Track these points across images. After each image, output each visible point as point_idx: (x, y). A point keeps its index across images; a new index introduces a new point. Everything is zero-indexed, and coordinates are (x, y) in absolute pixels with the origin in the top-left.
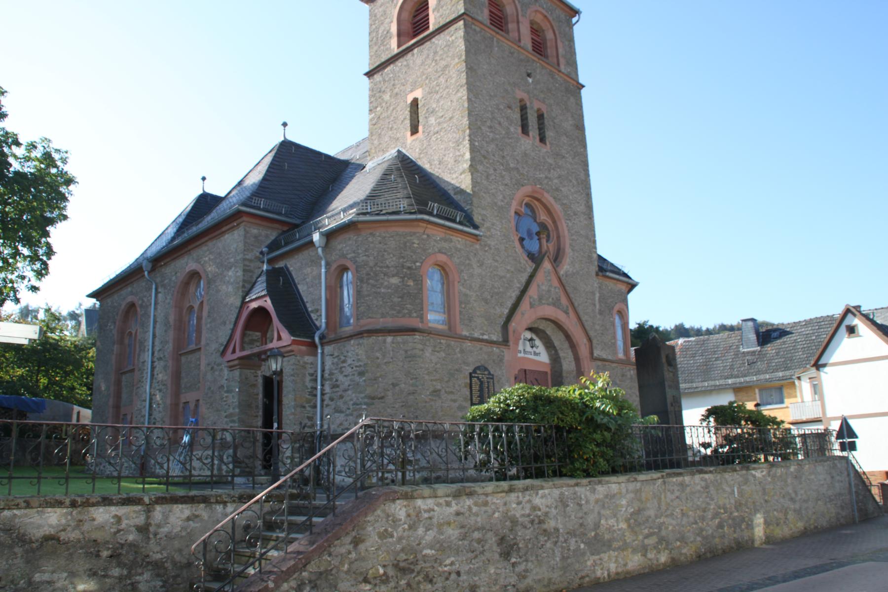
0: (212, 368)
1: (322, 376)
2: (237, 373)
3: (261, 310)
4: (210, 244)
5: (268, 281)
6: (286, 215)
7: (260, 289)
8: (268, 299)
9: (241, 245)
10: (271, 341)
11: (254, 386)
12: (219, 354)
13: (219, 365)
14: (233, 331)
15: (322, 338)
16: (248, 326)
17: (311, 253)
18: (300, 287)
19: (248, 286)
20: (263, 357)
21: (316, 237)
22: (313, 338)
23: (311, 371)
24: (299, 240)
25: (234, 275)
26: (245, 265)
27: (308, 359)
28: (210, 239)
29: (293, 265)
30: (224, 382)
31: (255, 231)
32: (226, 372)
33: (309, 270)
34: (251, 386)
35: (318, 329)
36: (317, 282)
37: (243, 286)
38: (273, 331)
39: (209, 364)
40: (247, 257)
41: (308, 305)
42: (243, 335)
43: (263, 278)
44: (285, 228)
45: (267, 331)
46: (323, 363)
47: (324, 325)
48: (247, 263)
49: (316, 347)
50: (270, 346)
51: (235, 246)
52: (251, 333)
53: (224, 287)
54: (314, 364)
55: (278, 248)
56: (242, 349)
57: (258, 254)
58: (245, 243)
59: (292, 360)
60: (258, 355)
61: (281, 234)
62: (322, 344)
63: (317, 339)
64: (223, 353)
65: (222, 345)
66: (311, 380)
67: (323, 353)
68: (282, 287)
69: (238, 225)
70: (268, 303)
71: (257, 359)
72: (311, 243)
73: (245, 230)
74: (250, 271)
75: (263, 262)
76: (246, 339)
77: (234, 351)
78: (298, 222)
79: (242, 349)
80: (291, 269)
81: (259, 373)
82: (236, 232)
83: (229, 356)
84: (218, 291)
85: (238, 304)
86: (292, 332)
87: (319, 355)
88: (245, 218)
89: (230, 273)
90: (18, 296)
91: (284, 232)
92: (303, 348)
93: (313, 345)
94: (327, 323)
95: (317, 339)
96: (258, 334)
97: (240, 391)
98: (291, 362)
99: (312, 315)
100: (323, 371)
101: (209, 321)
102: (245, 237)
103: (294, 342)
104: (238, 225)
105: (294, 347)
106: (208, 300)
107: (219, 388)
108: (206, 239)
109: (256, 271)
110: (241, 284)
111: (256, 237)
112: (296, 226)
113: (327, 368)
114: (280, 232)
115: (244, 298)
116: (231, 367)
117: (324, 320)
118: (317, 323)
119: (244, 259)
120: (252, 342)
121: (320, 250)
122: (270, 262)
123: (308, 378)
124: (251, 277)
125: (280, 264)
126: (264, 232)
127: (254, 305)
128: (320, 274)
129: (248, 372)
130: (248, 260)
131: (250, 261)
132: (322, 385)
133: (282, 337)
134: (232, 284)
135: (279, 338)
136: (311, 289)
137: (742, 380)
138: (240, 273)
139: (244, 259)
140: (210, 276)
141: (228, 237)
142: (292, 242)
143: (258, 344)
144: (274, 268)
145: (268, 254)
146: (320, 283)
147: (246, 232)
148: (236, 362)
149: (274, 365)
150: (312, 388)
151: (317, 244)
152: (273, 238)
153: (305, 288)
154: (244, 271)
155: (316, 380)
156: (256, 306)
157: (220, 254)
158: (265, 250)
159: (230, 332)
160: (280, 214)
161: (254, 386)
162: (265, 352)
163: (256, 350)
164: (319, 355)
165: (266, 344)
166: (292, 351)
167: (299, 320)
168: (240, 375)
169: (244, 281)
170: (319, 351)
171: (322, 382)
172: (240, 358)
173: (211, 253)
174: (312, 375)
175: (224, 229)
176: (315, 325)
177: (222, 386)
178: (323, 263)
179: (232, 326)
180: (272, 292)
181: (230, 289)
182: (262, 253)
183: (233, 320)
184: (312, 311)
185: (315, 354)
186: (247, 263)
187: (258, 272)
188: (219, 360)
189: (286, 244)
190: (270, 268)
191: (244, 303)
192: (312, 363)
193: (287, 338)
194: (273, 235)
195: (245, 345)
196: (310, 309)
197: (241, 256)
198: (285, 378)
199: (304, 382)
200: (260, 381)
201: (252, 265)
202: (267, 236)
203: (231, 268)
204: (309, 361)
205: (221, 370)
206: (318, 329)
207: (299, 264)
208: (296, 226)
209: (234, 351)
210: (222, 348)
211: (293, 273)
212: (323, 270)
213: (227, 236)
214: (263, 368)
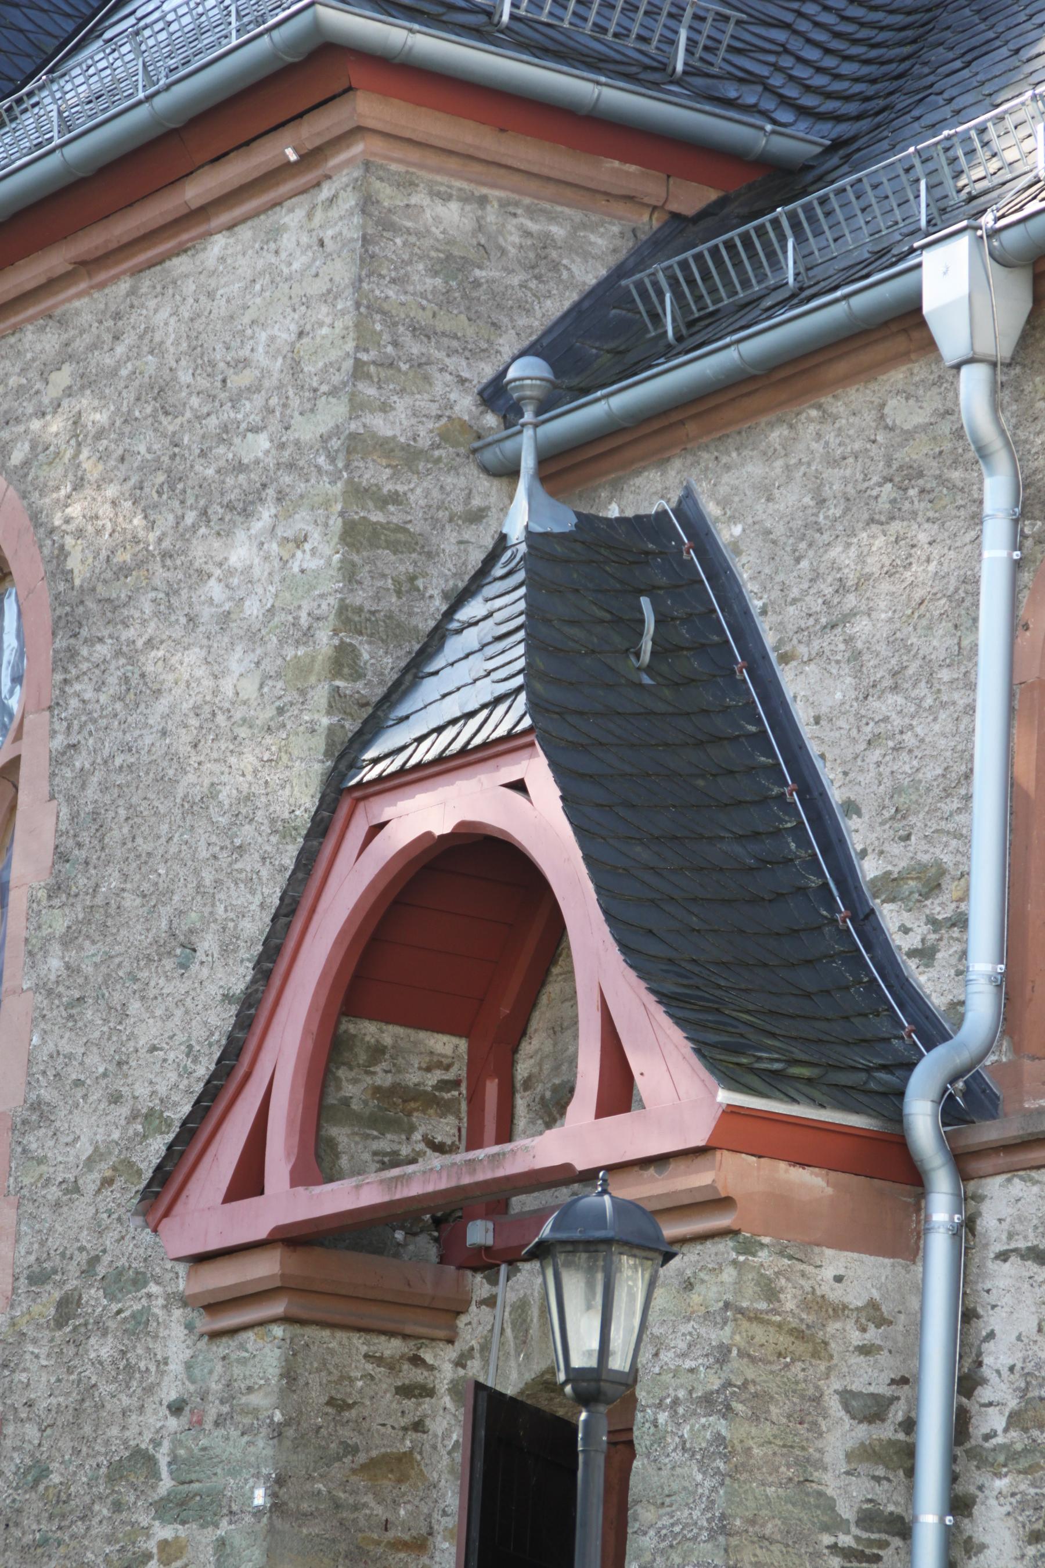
0: (67, 1308)
1: (959, 1426)
2: (264, 1354)
3: (482, 859)
4: (85, 307)
5: (539, 630)
6: (701, 85)
7: (479, 678)
8: (536, 768)
9: (333, 336)
10: (554, 1109)
11: (399, 1466)
12: (126, 1195)
13: (126, 1281)
14: (252, 1012)
15: (966, 1104)
16: (367, 981)
17: (904, 414)
18: (795, 684)
19: (383, 662)
20: (479, 1233)
21: (949, 280)
22: (891, 1102)
23: (870, 1378)
24: (799, 296)
25: (275, 565)
26: (357, 492)
27: (850, 1274)
28: (88, 266)
29: (760, 505)
30: (154, 1425)
31: (445, 215)
32: (175, 1341)
33: (877, 545)
34: (371, 1467)
35: (933, 1031)
36: (939, 643)
37: (344, 661)
38: (566, 1027)
39: (39, 1278)
40: (381, 425)
41: (857, 834)
42: (329, 1052)
43: (503, 604)
44: (692, 197)
45: (516, 1032)
46: (966, 1316)
47: (981, 1009)
48: (375, 473)
49: (915, 1179)
50: (542, 1149)
51: (284, 332)
52: (389, 1034)
53: (190, 661)
54: (889, 1322)
55: (629, 367)
56: (317, 1163)
57: (465, 404)
58: (367, 308)
59: (712, 1274)
60: (441, 1218)
61: (654, 247)
62: (964, 1163)
63: (921, 1117)
64: (162, 1191)
65: (152, 1118)
66: (865, 1454)
67: (967, 1229)
68: (659, 679)
69: (311, 157)
70: (537, 815)
71: (426, 1247)
72: (905, 324)
73: (367, 204)
74: (401, 540)
75: (510, 472)
76: (353, 1088)
77: (248, 1182)
78: (794, 140)
79: (317, 1163)
80: (727, 534)
81: (444, 1365)
82: (292, 217)
83: (207, 1215)
84: (138, 691)
85: (301, 798)
86: (723, 1052)
87: (939, 1248)
88: (367, 107)
89: (240, 552)
90: (1013, 1258)
91: (679, 228)
92: (810, 1182)
93: (891, 1163)
94: (1010, 990)
95: (921, 1117)
96: (447, 1045)
97: (277, 1506)
98: (710, 1293)
99: (890, 916)
100: (966, 1382)
101: (59, 922)
102: (368, 260)
103: (735, 1132)
104: (311, 157)
105: (735, 1172)
106: (57, 760)
107: (117, 1472)
108: (55, 260)
109: (448, 541)
110: (325, 640)
111: (452, 264)
112: (781, 180)
113: (997, 1357)
114: (648, 223)
115: (346, 754)
116: (214, 1307)
117: (983, 962)
118: (932, 984)
119: (357, 445)
120: (395, 1108)
121: (973, 387)
122: (560, 468)
123: (840, 1436)
124: (408, 587)
125: (643, 494)
126: (515, 226)
127: (424, 815)
128: (971, 582)
129: (351, 1354)
130: (385, 447)
131: (407, 457)
132: (959, 1505)
133: (641, 1090)
134: (253, 637)
135: (619, 1093)
136: (887, 705)
137: (623, 1305)
138: (320, 555)
139: (357, 445)
140: (79, 564)
141: (226, 262)
142: (748, 312)
143: (445, 1129)
144: (585, 521)
145: (547, 405)
146: (965, 655)
147: (378, 221)
148: (265, 1268)
149: (586, 1324)
150: (869, 1518)
151: (952, 336)
152: (588, 274)
153: (840, 691)
154: (354, 535)
155: (905, 1457)
156: (442, 827)
157: (160, 392)
158: (528, 372)
159: (222, 1020)
160: (650, 74)
161: (399, 1466)
162: (495, 1198)
163: (429, 1177)
164: (939, 1248)
165: (506, 1134)
166: (723, 1203)
167: (782, 959)
168: (290, 1376)
169: (349, 618)
170: (941, 1210)
171: (952, 1478)
172: (292, 1239)
173: (86, 383)
174: (871, 1409)
175: (195, 191)
176: (910, 998)
177: (143, 1459)
178: (996, 492)
179: (238, 977)
180: (574, 714)
181: (239, 675)
182: (496, 395)
183: (255, 926)
184: (890, 886)
185: (905, 1243)
186: (375, 473)
187: (459, 551)
188: (130, 1243)
189: (699, 329)
190: (561, 520)
191: (343, 793)
192: (874, 1314)
193: (679, 1093)
194: (590, 250)
195: (340, 1134)
196: (869, 869)
197: (332, 413)
198: (650, 1421)
199: (808, 1465)
200: (448, 1427)
201: (419, 490)
202: (541, 259)
203: (246, 511)
204: (855, 1296)
205: (140, 1325)
206: (933, 1031)
207: (792, 498)
208: (781, 180)
209: (248, 1182)
210: (157, 1146)
211: (747, 571)
212: (995, 552)
213: (219, 244)
214: (473, 1326)
